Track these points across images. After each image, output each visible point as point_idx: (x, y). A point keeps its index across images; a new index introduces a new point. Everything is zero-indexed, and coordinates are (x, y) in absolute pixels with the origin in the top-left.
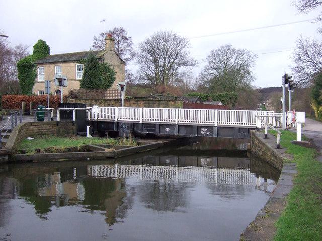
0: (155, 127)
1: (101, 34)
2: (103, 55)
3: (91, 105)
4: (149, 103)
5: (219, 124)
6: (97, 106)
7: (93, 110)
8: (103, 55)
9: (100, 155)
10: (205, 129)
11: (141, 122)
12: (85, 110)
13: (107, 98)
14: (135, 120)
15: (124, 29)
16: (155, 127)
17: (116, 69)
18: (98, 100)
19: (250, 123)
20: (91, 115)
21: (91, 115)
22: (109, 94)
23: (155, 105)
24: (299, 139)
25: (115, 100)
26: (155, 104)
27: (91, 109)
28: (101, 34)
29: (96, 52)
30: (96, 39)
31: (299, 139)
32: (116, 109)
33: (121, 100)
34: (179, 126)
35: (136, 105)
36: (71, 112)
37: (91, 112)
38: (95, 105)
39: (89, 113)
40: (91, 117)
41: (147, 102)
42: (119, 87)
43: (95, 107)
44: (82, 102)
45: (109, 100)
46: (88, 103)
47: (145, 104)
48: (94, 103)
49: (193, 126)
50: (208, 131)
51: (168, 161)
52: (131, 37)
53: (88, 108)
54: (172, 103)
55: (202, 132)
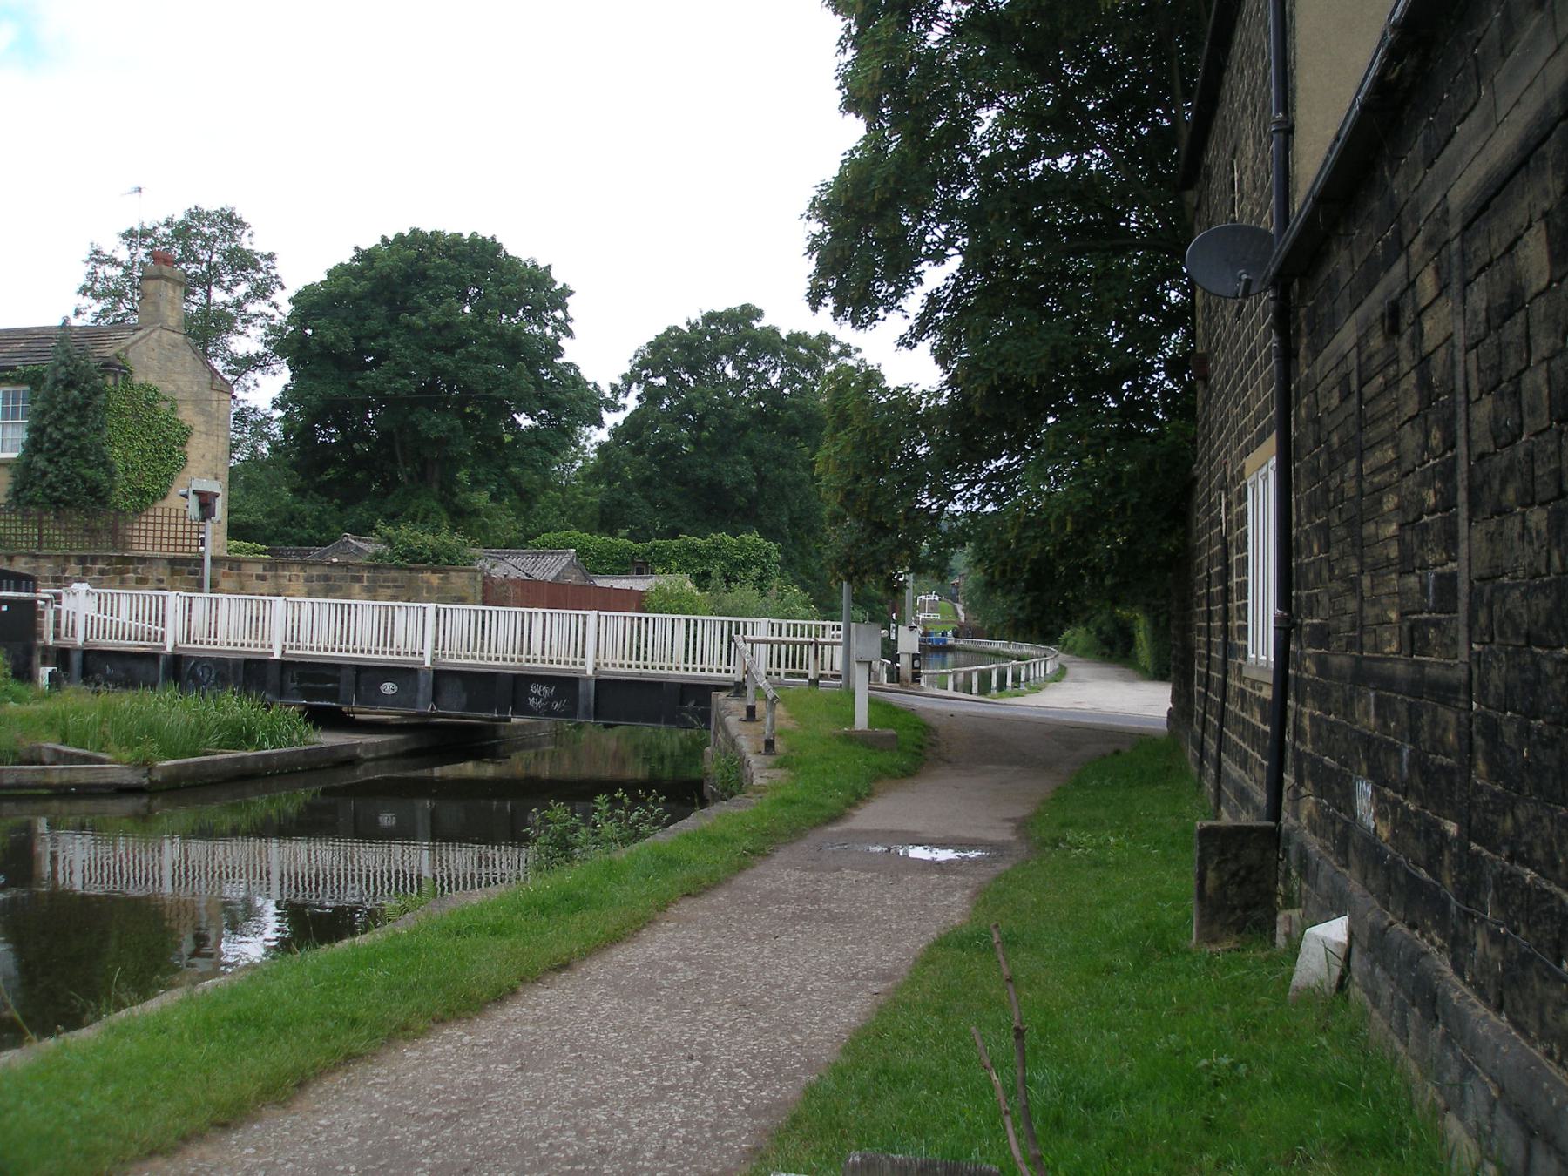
0: (336, 680)
1: (124, 236)
2: (126, 350)
3: (59, 580)
4: (327, 578)
5: (288, 651)
6: (84, 587)
7: (67, 604)
8: (126, 350)
9: (91, 779)
10: (546, 691)
11: (277, 656)
12: (33, 603)
13: (137, 551)
14: (255, 648)
15: (241, 213)
16: (336, 680)
17: (187, 415)
18: (94, 559)
19: (641, 662)
20: (57, 624)
21: (57, 624)
22: (145, 537)
23: (357, 587)
24: (861, 720)
25: (173, 562)
26: (359, 579)
27: (58, 597)
28: (124, 236)
29: (91, 335)
30: (98, 258)
31: (861, 720)
32: (174, 600)
33: (200, 562)
34: (441, 676)
35: (265, 586)
36: (990, 671)
37: (58, 613)
38: (80, 581)
39: (50, 613)
40: (57, 636)
41: (315, 571)
42: (193, 502)
43: (82, 588)
44: (21, 566)
45: (143, 560)
46: (46, 568)
47: (308, 579)
48: (74, 569)
49: (661, 683)
50: (557, 696)
51: (387, 820)
52: (271, 257)
53: (45, 593)
54: (435, 579)
55: (532, 701)
